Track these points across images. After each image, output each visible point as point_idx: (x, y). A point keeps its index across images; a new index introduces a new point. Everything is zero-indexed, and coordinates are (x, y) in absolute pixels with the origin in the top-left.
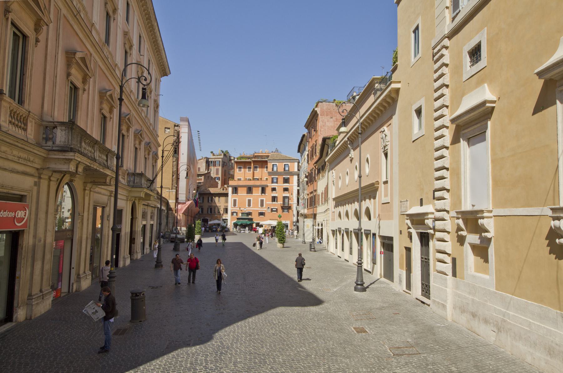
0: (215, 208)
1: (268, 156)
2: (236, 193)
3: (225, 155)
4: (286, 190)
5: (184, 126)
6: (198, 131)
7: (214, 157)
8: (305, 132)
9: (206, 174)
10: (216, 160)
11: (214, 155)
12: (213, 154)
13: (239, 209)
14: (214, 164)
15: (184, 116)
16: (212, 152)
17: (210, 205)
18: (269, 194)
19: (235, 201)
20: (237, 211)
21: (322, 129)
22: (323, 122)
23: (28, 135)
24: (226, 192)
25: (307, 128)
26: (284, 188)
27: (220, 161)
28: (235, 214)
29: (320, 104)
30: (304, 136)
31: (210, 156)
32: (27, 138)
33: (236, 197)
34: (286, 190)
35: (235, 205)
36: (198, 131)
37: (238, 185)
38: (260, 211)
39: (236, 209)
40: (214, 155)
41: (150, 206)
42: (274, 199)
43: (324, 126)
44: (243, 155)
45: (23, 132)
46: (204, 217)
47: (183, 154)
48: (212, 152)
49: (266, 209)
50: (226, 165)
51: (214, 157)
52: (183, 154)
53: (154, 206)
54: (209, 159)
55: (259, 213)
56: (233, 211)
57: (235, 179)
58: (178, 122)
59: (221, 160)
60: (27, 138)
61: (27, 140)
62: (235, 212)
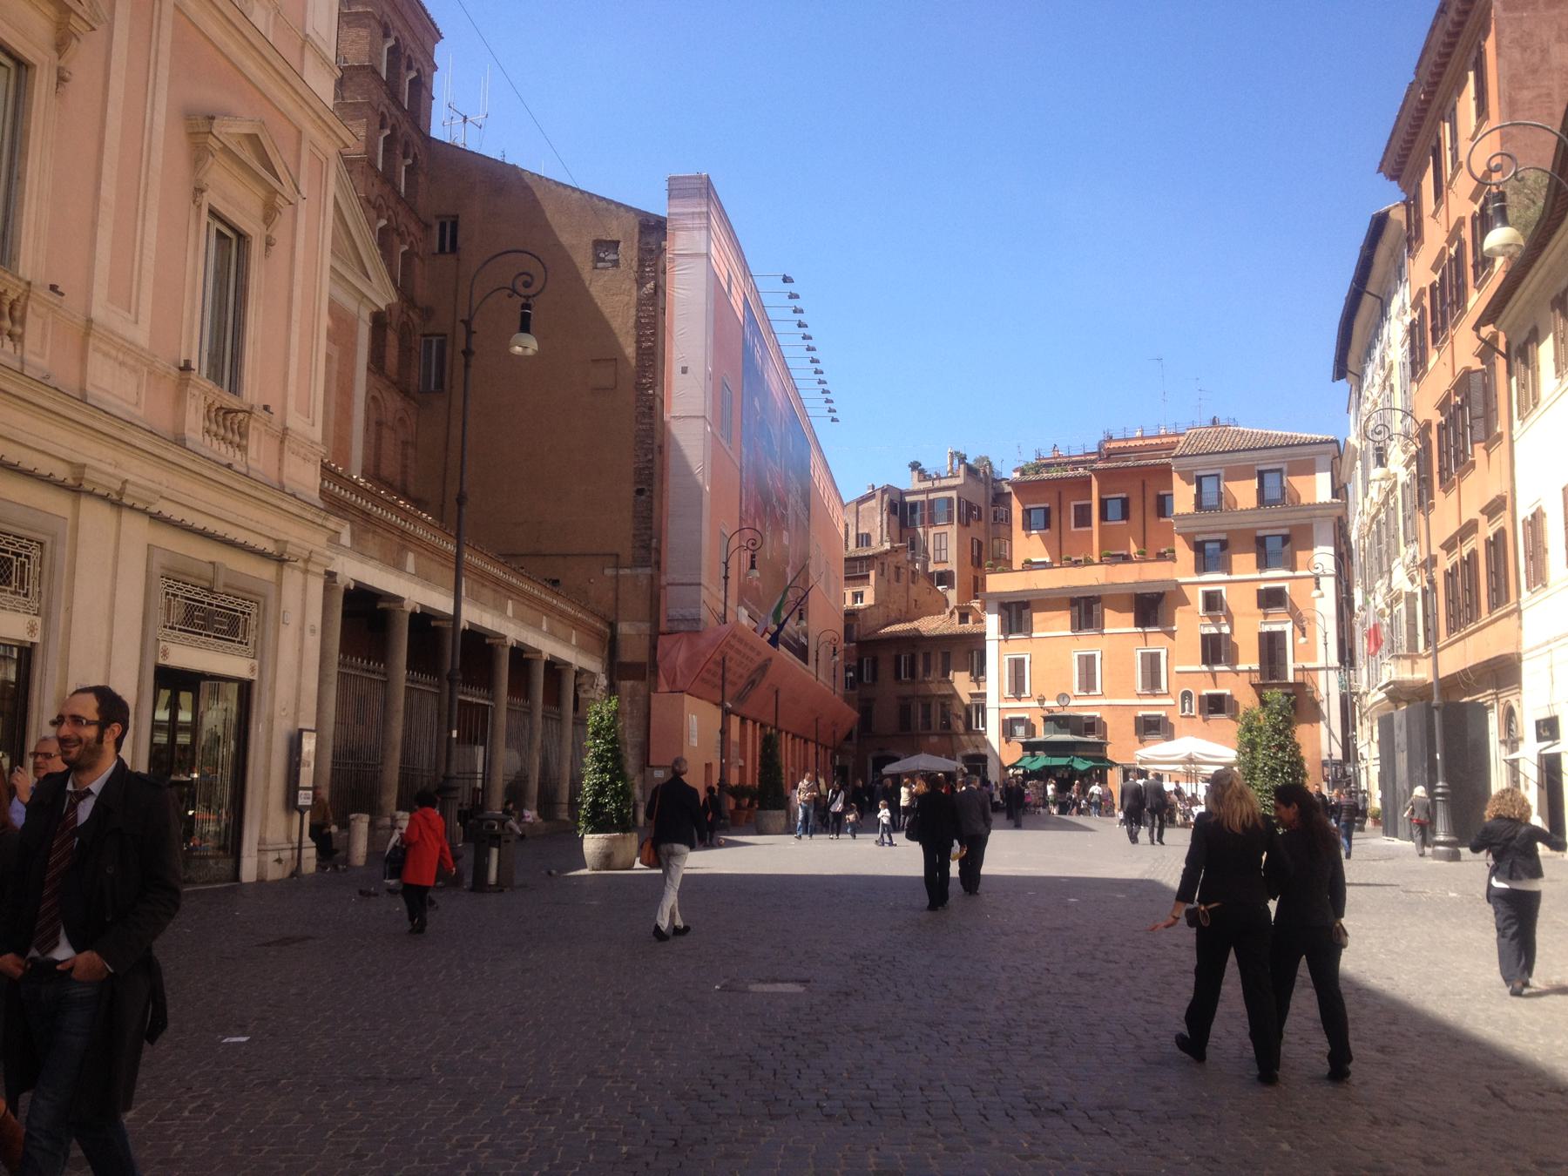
0: (927, 708)
1: (1172, 447)
2: (1019, 631)
3: (971, 471)
4: (1271, 599)
5: (689, 223)
6: (786, 280)
7: (928, 484)
8: (1390, 198)
9: (886, 553)
10: (932, 496)
11: (923, 475)
12: (922, 472)
13: (1036, 704)
14: (931, 513)
15: (687, 168)
16: (915, 466)
17: (906, 690)
18: (1191, 623)
19: (1017, 666)
20: (1027, 716)
21: (1526, 95)
22: (1524, 49)
23: (249, 462)
24: (975, 630)
25: (1395, 176)
26: (1259, 592)
27: (950, 500)
28: (1020, 730)
29: (1379, 301)
30: (1379, 223)
31: (907, 481)
32: (22, 362)
33: (1019, 646)
34: (1271, 599)
35: (1017, 688)
36: (786, 280)
37: (1026, 588)
38: (1140, 714)
39: (1027, 708)
40: (923, 475)
41: (91, 494)
42: (1215, 650)
43: (1534, 71)
44: (1048, 454)
45: (238, 454)
46: (881, 749)
47: (684, 370)
48: (915, 466)
49: (1171, 701)
50: (980, 519)
51: (928, 484)
52: (684, 370)
53: (270, 548)
54: (902, 494)
55: (1137, 718)
56: (1007, 716)
57: (1014, 568)
58: (657, 205)
59: (953, 494)
60: (22, 362)
61: (22, 370)
62: (1021, 721)
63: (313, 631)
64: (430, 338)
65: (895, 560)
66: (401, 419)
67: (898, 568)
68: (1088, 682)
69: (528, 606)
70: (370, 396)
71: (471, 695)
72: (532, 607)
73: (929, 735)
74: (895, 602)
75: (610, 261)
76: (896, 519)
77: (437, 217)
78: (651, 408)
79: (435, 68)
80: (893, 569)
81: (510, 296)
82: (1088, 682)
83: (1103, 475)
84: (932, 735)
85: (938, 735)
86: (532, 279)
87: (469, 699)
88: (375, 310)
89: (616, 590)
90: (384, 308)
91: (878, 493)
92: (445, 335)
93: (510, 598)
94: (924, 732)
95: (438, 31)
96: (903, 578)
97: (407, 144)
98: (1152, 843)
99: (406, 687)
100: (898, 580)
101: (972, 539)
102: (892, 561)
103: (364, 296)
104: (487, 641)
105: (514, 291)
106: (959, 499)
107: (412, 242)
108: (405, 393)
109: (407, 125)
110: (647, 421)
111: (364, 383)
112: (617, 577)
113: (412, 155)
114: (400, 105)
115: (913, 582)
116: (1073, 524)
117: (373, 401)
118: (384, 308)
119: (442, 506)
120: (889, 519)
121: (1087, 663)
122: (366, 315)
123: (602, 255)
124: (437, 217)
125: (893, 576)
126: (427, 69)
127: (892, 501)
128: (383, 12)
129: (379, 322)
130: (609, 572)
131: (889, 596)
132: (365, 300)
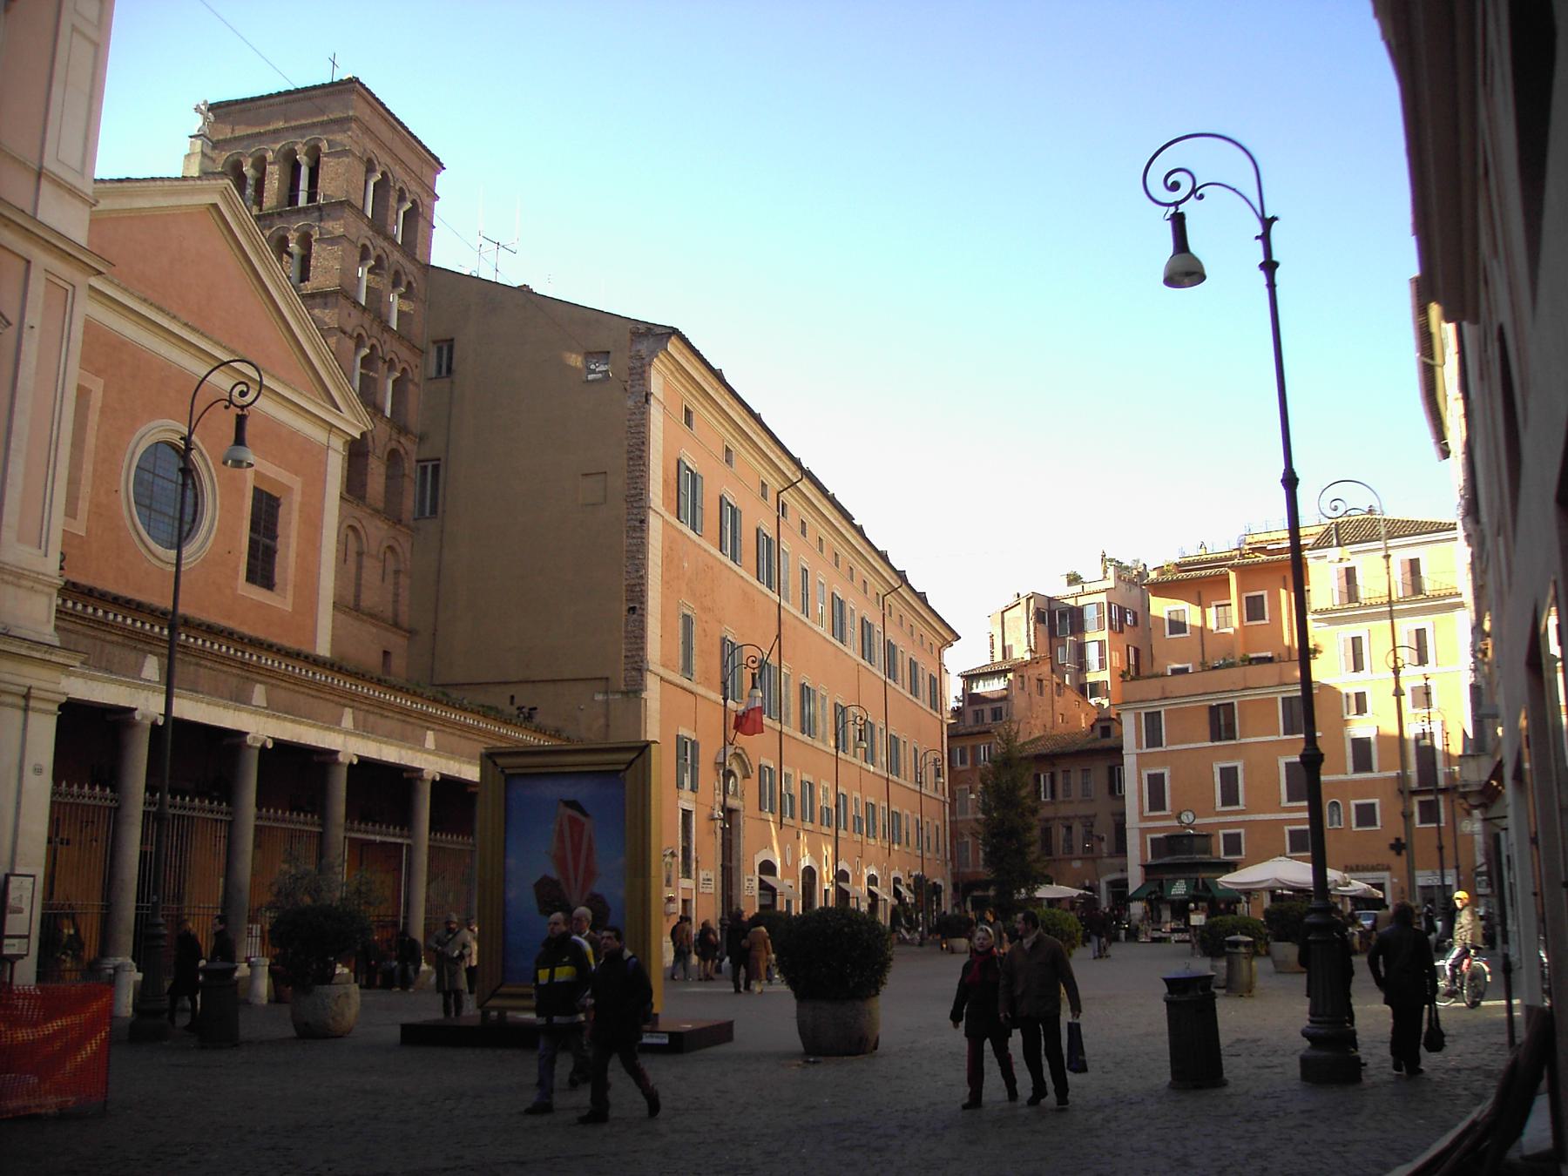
31: (1058, 589)
63: (38, 770)
64: (426, 464)
65: (1036, 672)
66: (391, 548)
67: (1040, 681)
68: (1230, 797)
69: (460, 736)
70: (345, 525)
71: (374, 833)
72: (465, 738)
73: (1072, 859)
74: (1037, 717)
75: (600, 372)
76: (1044, 628)
77: (435, 342)
78: (642, 521)
79: (436, 198)
80: (1034, 682)
81: (227, 407)
82: (1230, 797)
83: (1244, 571)
84: (1075, 859)
85: (1080, 859)
86: (248, 390)
87: (372, 837)
88: (349, 438)
89: (607, 716)
90: (358, 437)
91: (1023, 601)
92: (439, 460)
93: (428, 728)
94: (1067, 856)
95: (437, 159)
96: (1047, 691)
97: (397, 273)
98: (737, 991)
99: (256, 826)
100: (1041, 694)
101: (1128, 646)
102: (1033, 673)
103: (332, 426)
104: (405, 775)
105: (231, 402)
106: (1109, 604)
107: (404, 369)
108: (395, 519)
109: (396, 253)
110: (638, 535)
111: (337, 512)
112: (607, 702)
113: (404, 283)
114: (393, 241)
115: (1059, 695)
116: (1263, 622)
117: (350, 531)
118: (358, 437)
119: (434, 634)
120: (1035, 629)
121: (1229, 776)
122: (338, 444)
123: (593, 367)
124: (435, 342)
125: (1034, 689)
126: (427, 200)
127: (1038, 609)
128: (365, 150)
129: (357, 451)
130: (599, 697)
131: (1031, 710)
132: (334, 429)
